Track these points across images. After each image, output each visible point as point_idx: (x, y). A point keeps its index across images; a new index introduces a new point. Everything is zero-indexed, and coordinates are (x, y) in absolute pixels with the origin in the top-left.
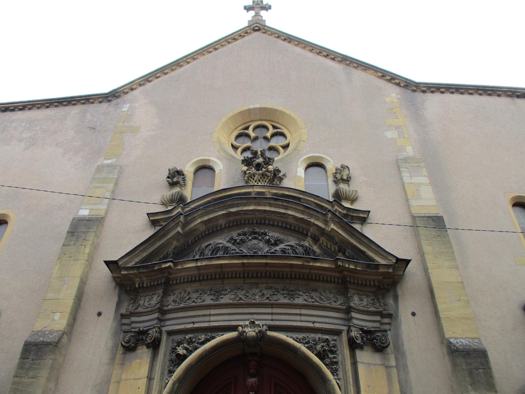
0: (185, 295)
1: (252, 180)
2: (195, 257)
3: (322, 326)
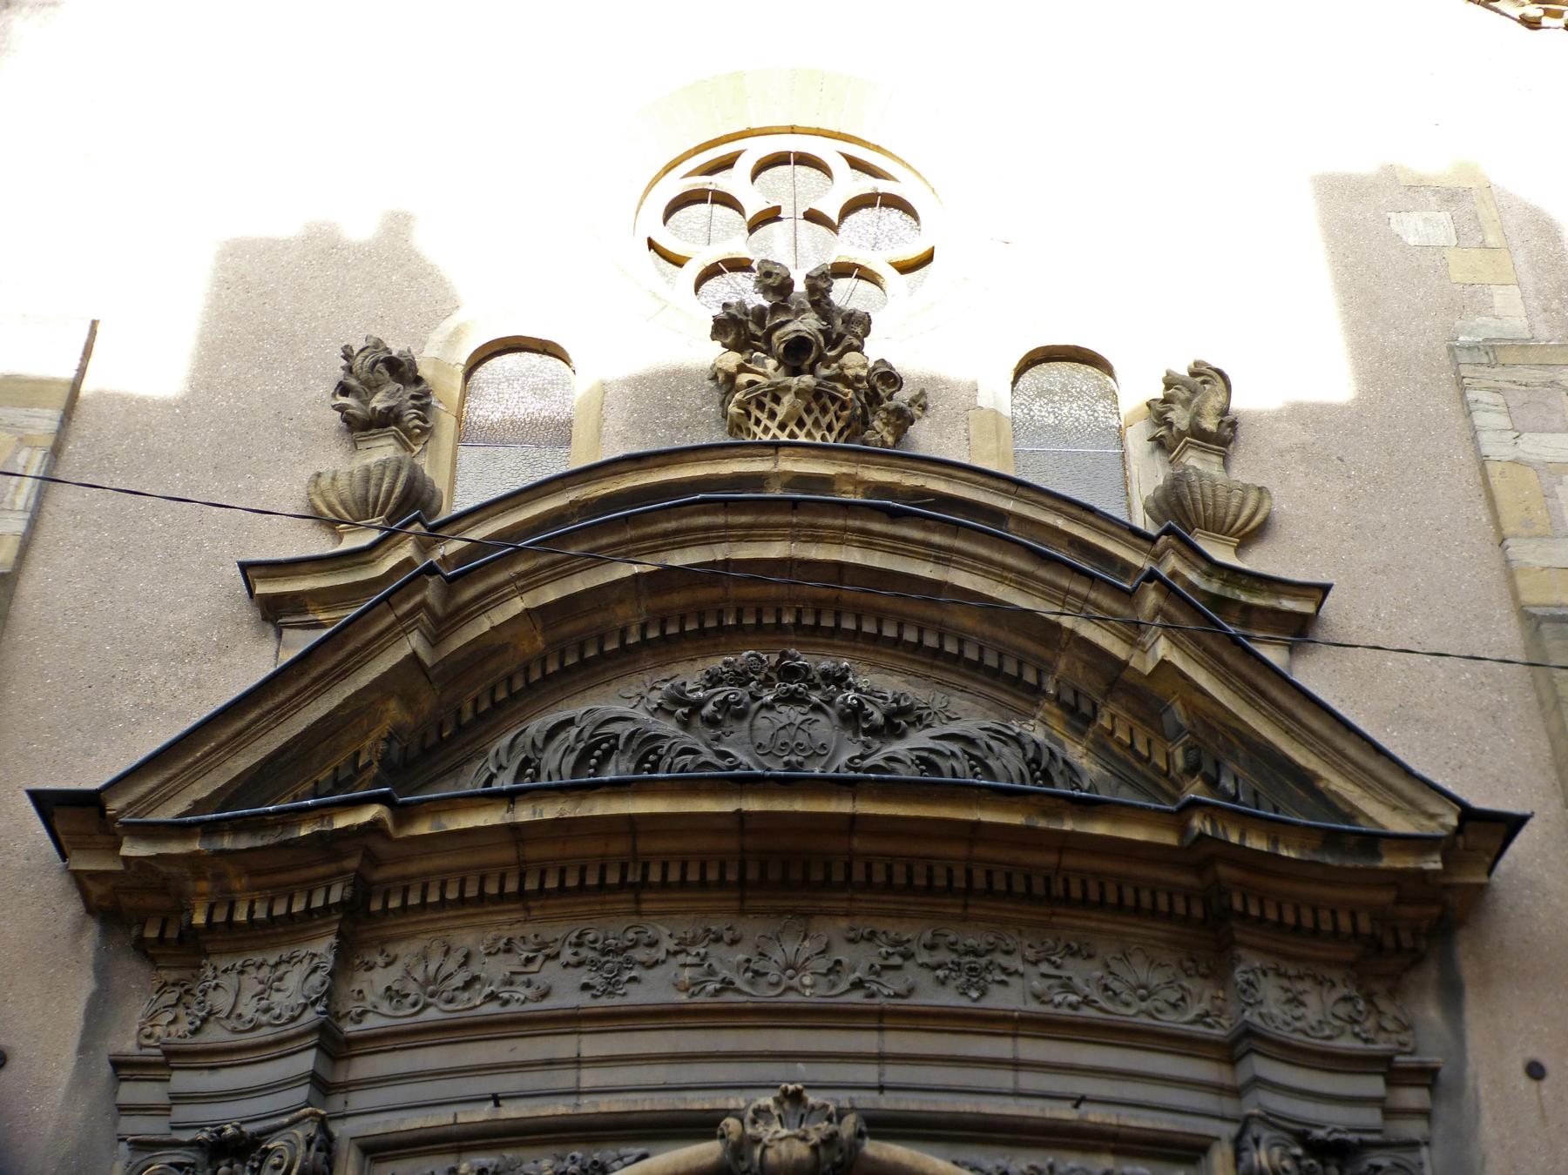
0: (451, 965)
1: (763, 417)
2: (494, 781)
3: (1118, 1116)
